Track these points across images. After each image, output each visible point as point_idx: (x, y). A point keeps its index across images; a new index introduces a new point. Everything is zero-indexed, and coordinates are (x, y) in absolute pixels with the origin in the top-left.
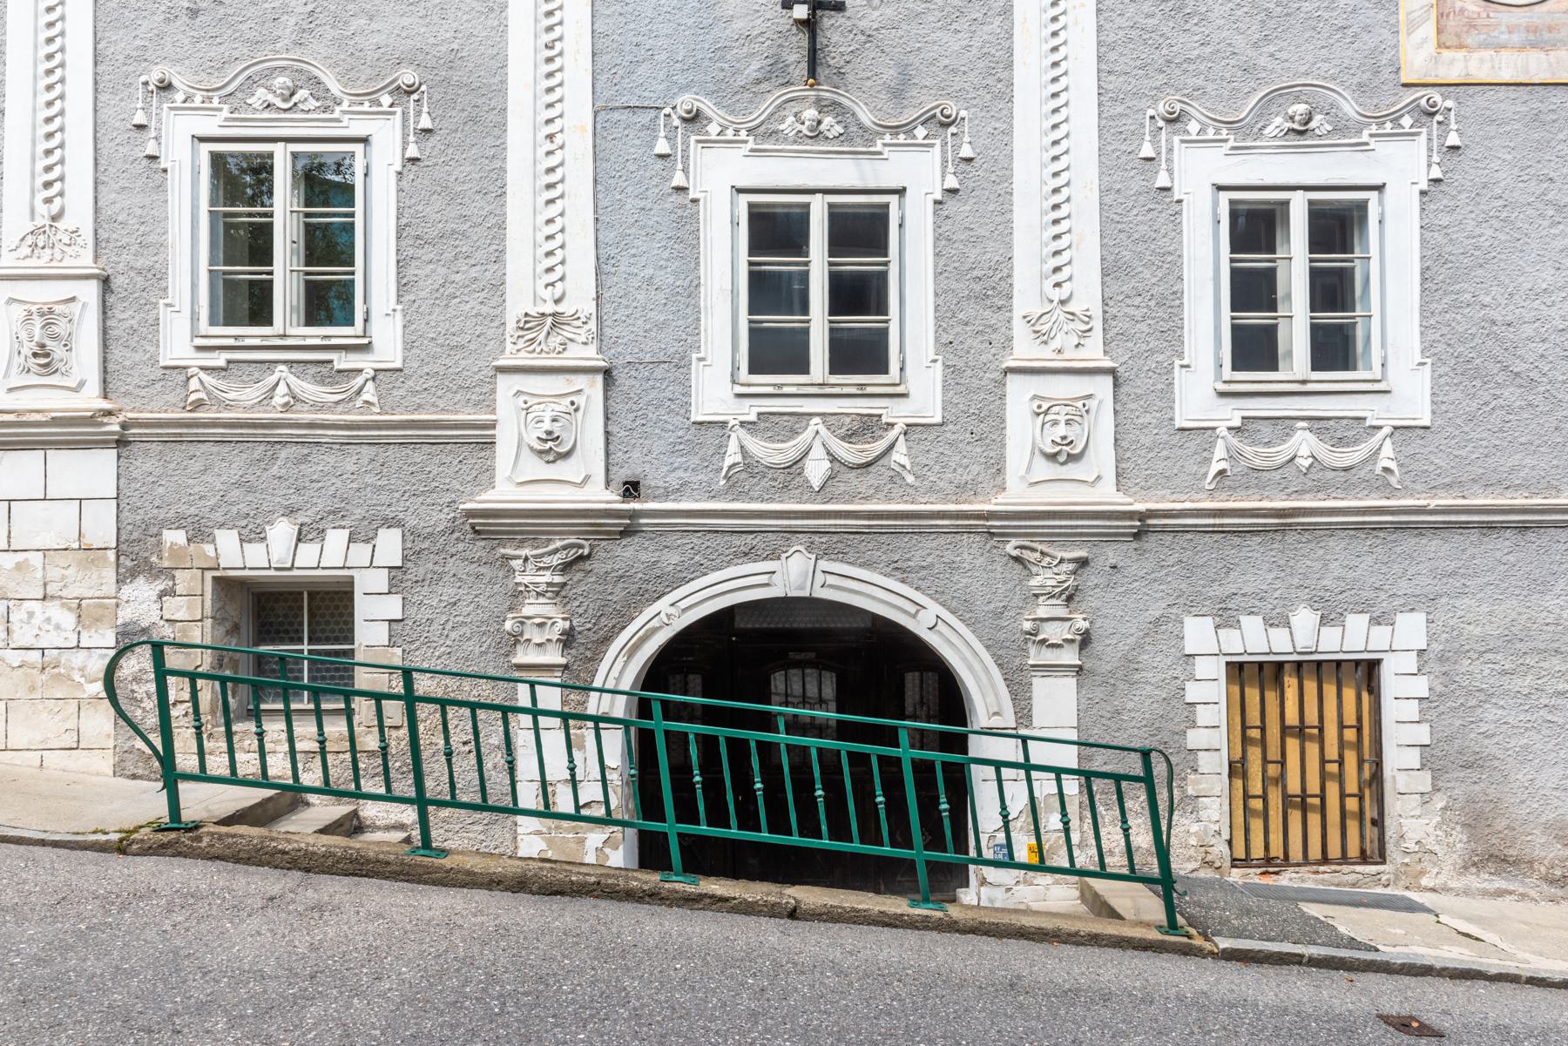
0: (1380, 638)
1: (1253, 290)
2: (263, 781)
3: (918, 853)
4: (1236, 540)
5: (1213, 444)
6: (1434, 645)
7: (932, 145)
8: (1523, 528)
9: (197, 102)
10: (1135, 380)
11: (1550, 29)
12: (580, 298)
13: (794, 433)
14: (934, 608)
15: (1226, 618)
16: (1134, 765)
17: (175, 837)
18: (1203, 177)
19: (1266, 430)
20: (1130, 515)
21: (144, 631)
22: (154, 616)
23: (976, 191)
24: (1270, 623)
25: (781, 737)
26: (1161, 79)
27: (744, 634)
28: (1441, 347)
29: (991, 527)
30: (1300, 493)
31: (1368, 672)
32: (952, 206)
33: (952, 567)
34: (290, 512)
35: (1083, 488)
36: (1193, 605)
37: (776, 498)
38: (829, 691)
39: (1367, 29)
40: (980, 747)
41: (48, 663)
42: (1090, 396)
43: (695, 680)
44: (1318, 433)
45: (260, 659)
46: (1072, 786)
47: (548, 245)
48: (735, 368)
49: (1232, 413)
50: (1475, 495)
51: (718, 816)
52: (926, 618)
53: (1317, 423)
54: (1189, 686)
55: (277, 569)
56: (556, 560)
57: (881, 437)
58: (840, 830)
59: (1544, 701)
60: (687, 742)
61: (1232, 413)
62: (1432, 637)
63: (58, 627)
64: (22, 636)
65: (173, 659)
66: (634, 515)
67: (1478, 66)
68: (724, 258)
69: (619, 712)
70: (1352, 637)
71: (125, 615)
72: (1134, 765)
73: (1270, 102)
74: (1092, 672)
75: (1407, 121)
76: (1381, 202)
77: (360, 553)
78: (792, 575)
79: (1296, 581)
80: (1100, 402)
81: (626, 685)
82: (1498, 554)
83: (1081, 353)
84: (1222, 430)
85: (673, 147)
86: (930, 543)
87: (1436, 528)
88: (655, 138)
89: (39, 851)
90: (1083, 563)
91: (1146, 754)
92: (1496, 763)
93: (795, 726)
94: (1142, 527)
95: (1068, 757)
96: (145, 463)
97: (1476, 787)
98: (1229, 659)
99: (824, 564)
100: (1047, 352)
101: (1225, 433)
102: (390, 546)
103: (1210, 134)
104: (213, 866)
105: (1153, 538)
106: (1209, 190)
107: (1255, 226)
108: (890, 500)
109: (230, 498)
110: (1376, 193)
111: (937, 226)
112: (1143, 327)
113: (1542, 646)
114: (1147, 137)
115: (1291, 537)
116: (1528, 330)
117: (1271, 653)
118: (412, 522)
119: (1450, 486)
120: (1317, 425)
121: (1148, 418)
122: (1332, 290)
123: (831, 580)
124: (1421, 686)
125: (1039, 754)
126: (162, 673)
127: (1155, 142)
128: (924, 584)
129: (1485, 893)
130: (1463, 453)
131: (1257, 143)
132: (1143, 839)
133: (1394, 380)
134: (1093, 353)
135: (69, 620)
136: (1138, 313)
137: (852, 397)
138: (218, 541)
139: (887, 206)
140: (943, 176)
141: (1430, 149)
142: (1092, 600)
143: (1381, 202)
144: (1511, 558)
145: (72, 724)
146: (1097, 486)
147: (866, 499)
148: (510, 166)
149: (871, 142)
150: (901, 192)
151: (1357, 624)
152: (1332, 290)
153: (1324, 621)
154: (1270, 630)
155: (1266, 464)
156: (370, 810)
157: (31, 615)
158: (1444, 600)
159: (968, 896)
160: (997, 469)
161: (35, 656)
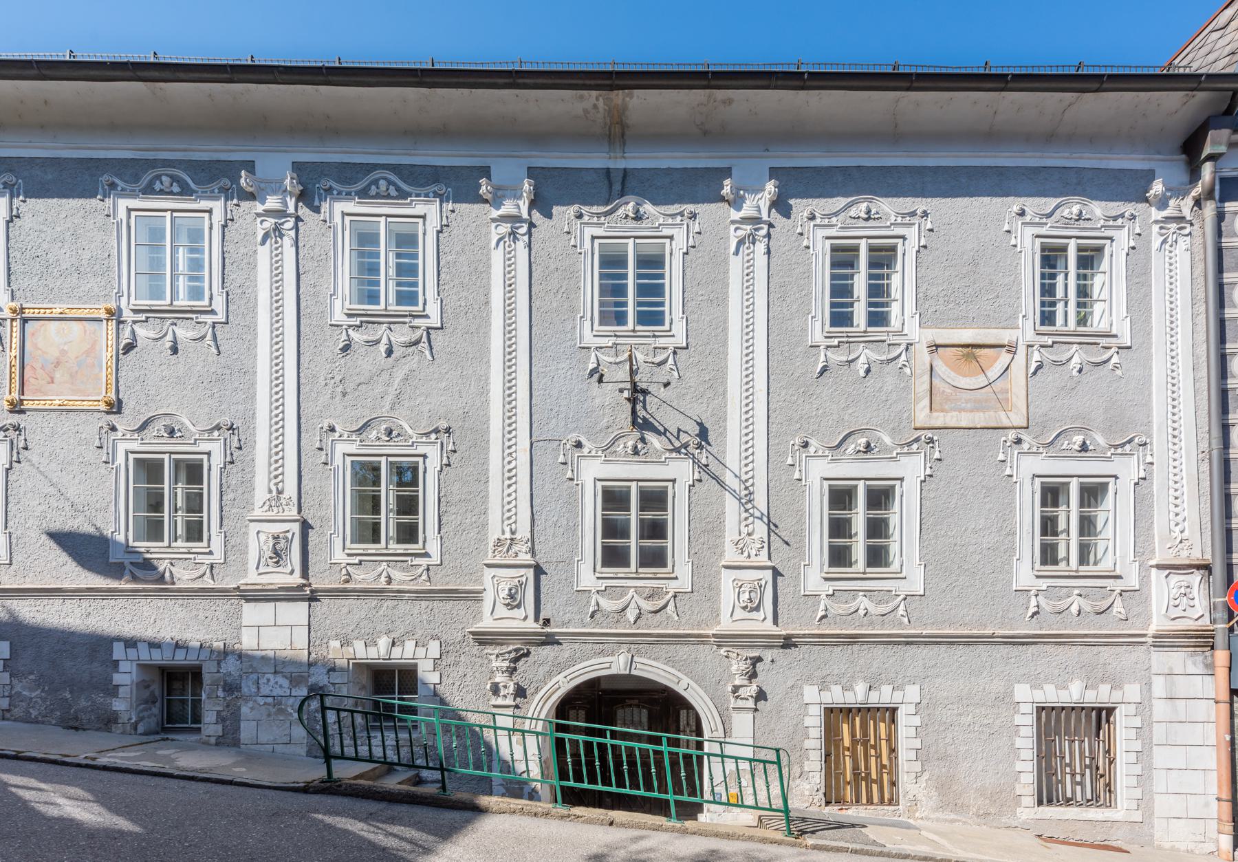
0: (898, 697)
1: (839, 528)
2: (370, 760)
3: (671, 797)
9: (345, 437)
13: (622, 596)
15: (823, 686)
16: (772, 756)
17: (330, 787)
18: (819, 472)
20: (779, 636)
21: (321, 688)
22: (325, 681)
25: (608, 741)
26: (798, 426)
27: (604, 691)
31: (892, 712)
34: (388, 632)
36: (809, 680)
37: (609, 627)
38: (645, 719)
40: (707, 747)
41: (277, 701)
43: (582, 713)
45: (376, 704)
46: (744, 766)
47: (504, 508)
48: (822, 565)
49: (829, 588)
51: (579, 778)
52: (683, 685)
58: (649, 787)
60: (578, 746)
61: (829, 588)
63: (281, 686)
64: (265, 690)
65: (328, 702)
67: (951, 419)
68: (591, 512)
69: (539, 729)
70: (883, 696)
71: (312, 680)
72: (772, 756)
77: (421, 652)
78: (616, 664)
81: (542, 716)
83: (758, 558)
86: (686, 648)
89: (267, 792)
91: (777, 751)
93: (614, 735)
94: (788, 643)
95: (748, 752)
96: (321, 608)
102: (434, 649)
103: (1034, 449)
104: (346, 800)
107: (841, 497)
109: (362, 625)
116: (971, 549)
118: (444, 637)
122: (877, 528)
123: (639, 666)
124: (917, 721)
125: (729, 750)
126: (324, 709)
129: (946, 820)
132: (776, 790)
135: (286, 683)
137: (649, 579)
145: (287, 732)
148: (491, 468)
149: (891, 452)
151: (886, 690)
152: (877, 528)
156: (425, 774)
157: (268, 680)
159: (702, 818)
161: (270, 700)
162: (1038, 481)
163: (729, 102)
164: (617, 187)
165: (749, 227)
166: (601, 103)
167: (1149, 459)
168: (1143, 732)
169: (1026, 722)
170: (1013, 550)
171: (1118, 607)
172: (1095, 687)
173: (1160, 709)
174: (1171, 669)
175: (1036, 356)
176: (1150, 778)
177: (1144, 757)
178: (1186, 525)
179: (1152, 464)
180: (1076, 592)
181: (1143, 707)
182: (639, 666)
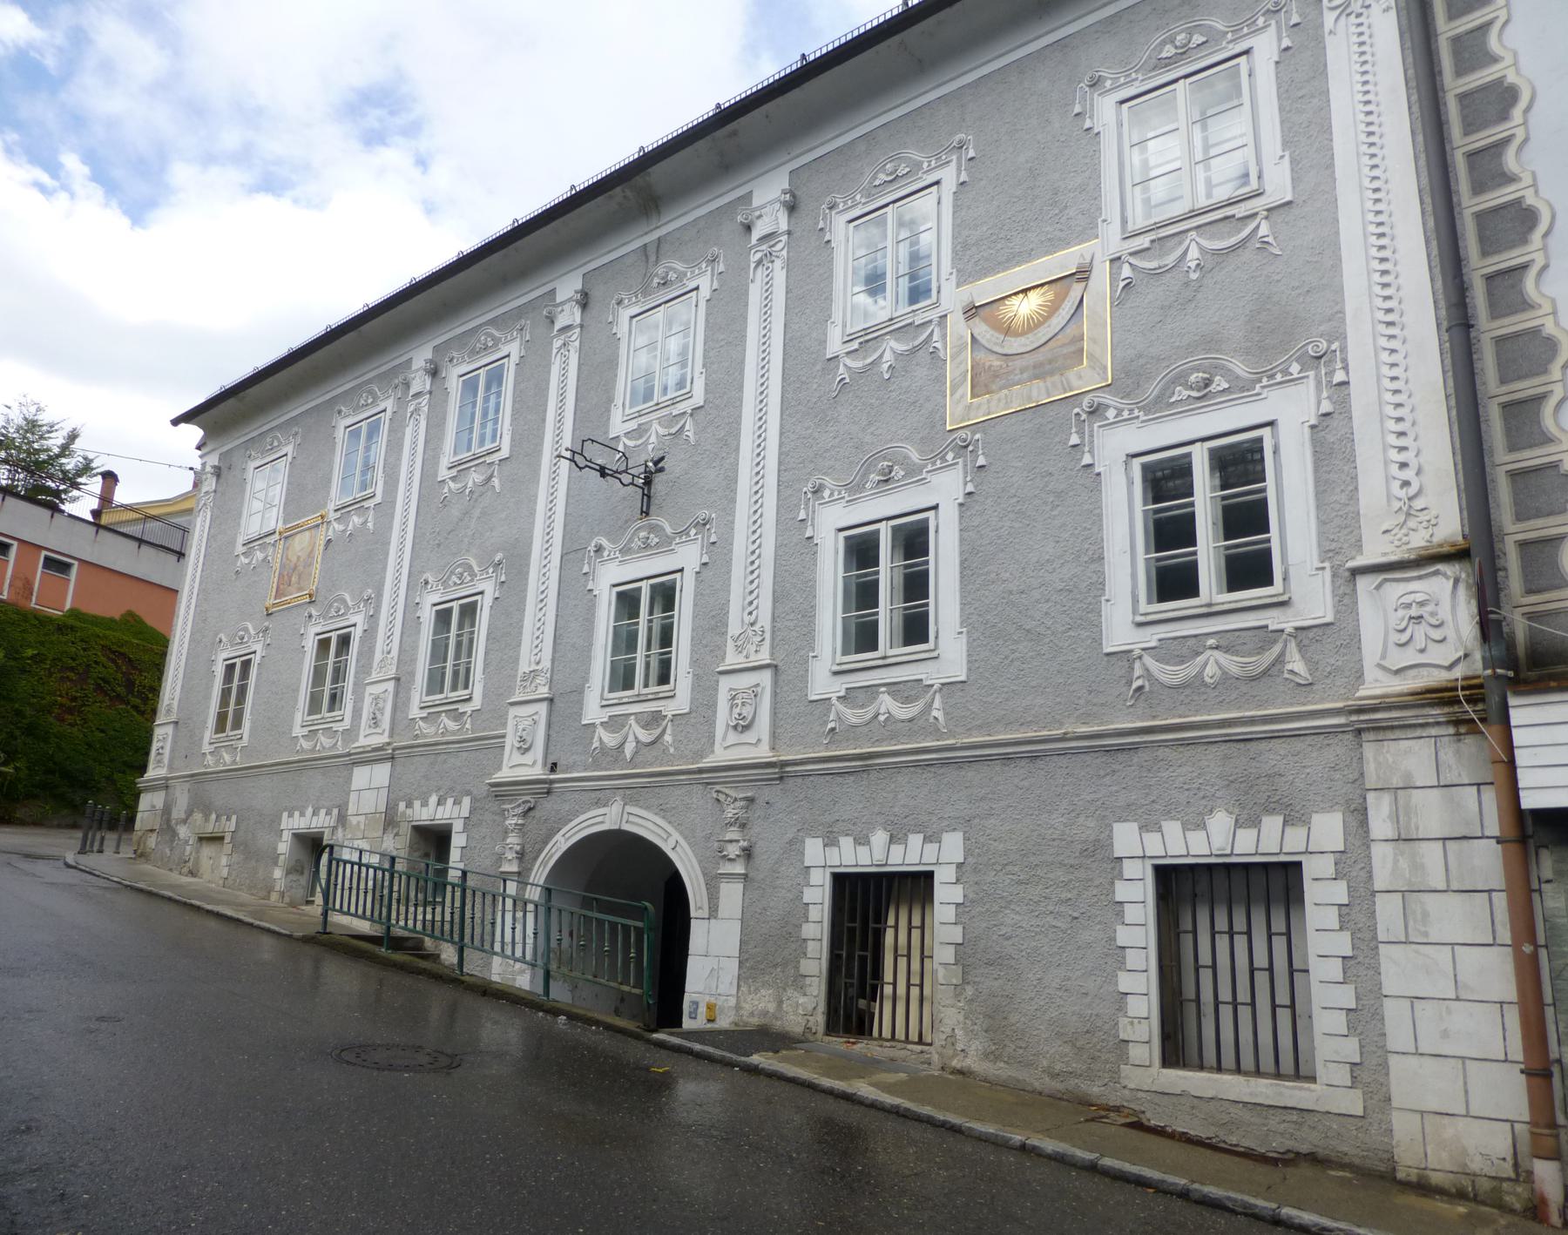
4: (839, 779)
5: (829, 710)
6: (970, 859)
8: (1034, 757)
10: (785, 671)
11: (1050, 362)
12: (546, 663)
14: (676, 836)
15: (831, 842)
18: (831, 523)
19: (861, 695)
23: (715, 567)
24: (857, 842)
28: (974, 617)
29: (710, 777)
30: (879, 741)
32: (707, 573)
36: (808, 829)
39: (928, 399)
48: (1135, 601)
50: (999, 733)
53: (894, 688)
54: (805, 890)
56: (520, 810)
59: (1051, 908)
62: (968, 852)
66: (552, 782)
70: (907, 856)
73: (868, 468)
74: (753, 880)
75: (950, 456)
76: (1275, 436)
79: (876, 809)
82: (1016, 781)
83: (760, 656)
84: (834, 701)
85: (1082, 438)
87: (972, 761)
90: (751, 800)
92: (1013, 963)
94: (779, 772)
97: (996, 984)
99: (629, 809)
100: (741, 658)
105: (791, 782)
107: (861, 551)
110: (1268, 429)
111: (697, 587)
112: (794, 633)
113: (1050, 859)
115: (874, 775)
116: (1036, 594)
119: (980, 727)
121: (794, 696)
123: (632, 818)
127: (1081, 433)
130: (989, 699)
133: (1296, 591)
136: (791, 624)
140: (1319, 403)
141: (966, 473)
143: (1275, 436)
144: (1026, 783)
147: (651, 765)
152: (865, 595)
153: (892, 840)
154: (1146, 836)
158: (977, 821)
162: (1137, 464)
163: (735, 133)
164: (653, 258)
165: (764, 247)
166: (628, 193)
167: (1339, 376)
168: (1357, 915)
169: (1137, 895)
170: (1101, 585)
171: (1296, 664)
172: (1255, 822)
173: (1384, 863)
174: (1408, 775)
175: (1126, 271)
176: (1378, 1016)
177: (1361, 965)
178: (1410, 479)
179: (1345, 383)
180: (1211, 642)
181: (1352, 861)
182: (632, 818)
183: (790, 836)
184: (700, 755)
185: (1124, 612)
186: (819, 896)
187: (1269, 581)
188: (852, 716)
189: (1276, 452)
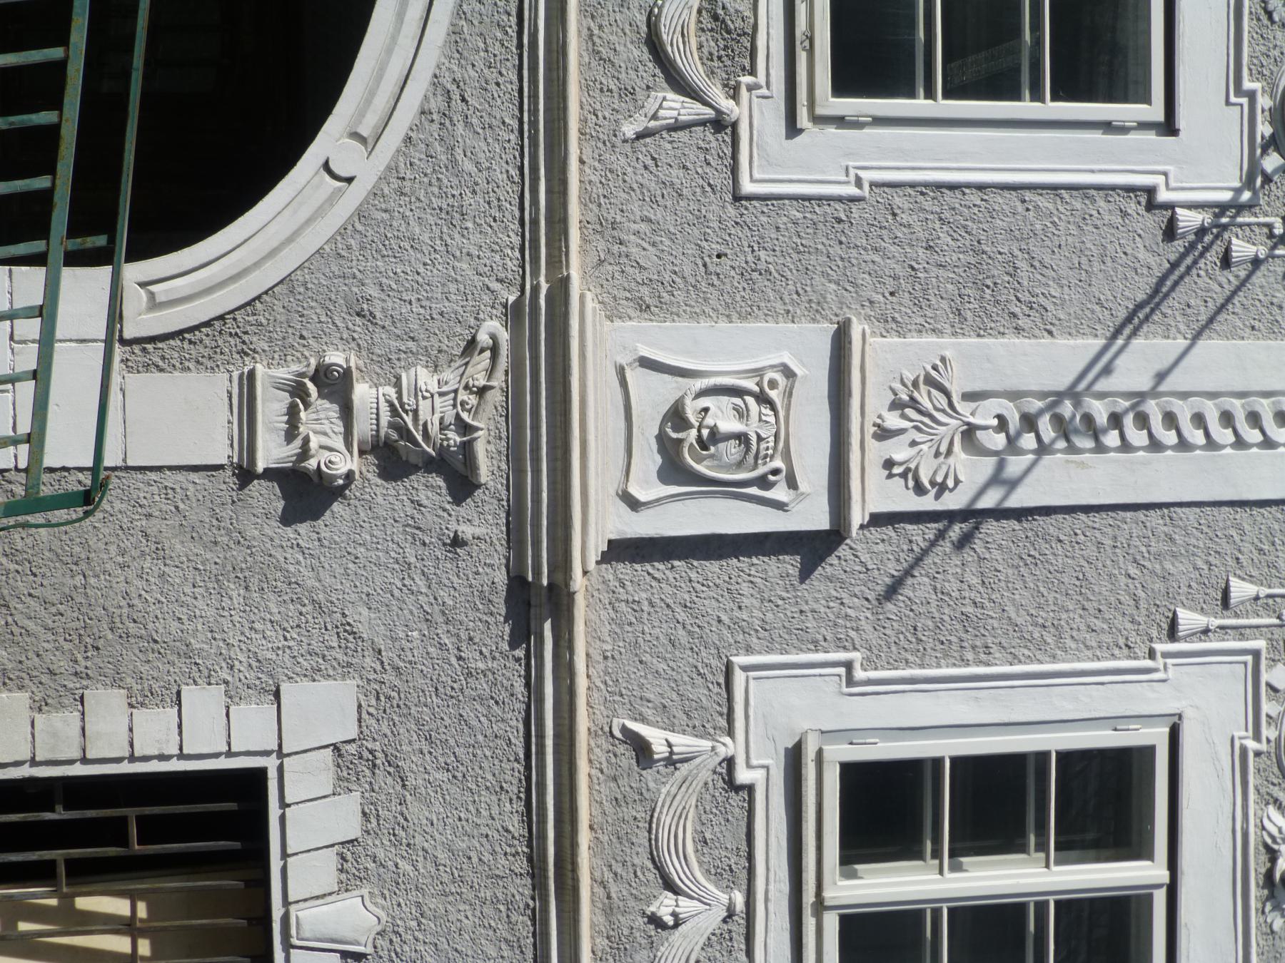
7: (1247, 730)
14: (368, 169)
15: (352, 762)
20: (561, 562)
33: (453, 215)
35: (617, 473)
36: (380, 701)
40: (84, 289)
42: (792, 483)
44: (719, 939)
49: (761, 770)
55: (286, 919)
57: (711, 73)
61: (761, 770)
80: (780, 506)
83: (876, 473)
84: (727, 746)
88: (1250, 578)
94: (535, 604)
98: (272, 775)
101: (723, 752)
106: (1171, 707)
108: (586, 87)
114: (1264, 591)
115: (521, 889)
117: (285, 855)
120: (738, 927)
128: (417, 155)
131: (1252, 796)
134: (875, 493)
138: (343, 798)
139: (1147, 99)
142: (386, 497)
146: (614, 492)
150: (1168, 127)
154: (331, 857)
155: (663, 836)
160: (649, 303)
162: (1157, 736)
183: (361, 617)
184: (614, 256)
185: (828, 703)
186: (198, 731)
187: (841, 87)
188: (679, 808)
189: (1107, 126)
